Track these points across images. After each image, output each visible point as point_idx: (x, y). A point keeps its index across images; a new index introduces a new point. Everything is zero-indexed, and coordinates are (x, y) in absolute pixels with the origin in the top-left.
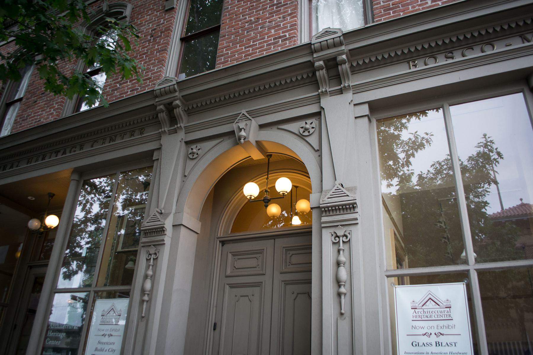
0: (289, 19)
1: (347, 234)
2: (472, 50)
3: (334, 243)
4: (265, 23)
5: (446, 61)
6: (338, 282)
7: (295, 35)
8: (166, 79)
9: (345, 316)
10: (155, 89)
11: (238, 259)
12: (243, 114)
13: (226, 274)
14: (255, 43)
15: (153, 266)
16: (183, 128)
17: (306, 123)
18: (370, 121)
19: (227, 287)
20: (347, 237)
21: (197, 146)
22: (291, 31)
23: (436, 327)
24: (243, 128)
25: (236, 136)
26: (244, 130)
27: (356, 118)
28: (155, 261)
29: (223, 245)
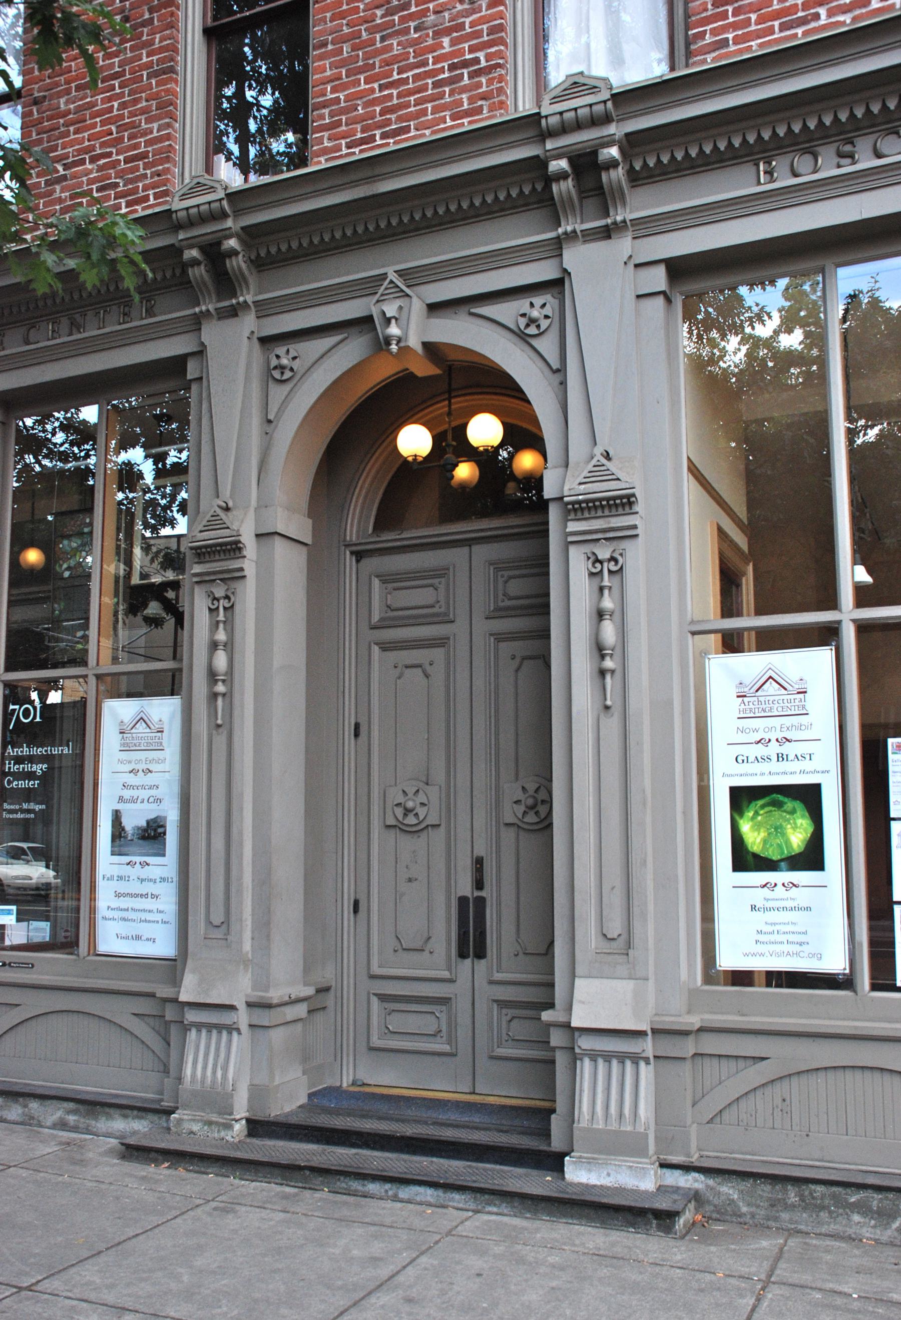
0: (484, 9)
1: (616, 555)
2: (894, 136)
3: (592, 574)
4: (424, 13)
5: (839, 166)
6: (600, 650)
7: (501, 61)
8: (198, 183)
9: (613, 709)
10: (175, 207)
11: (394, 589)
12: (391, 282)
13: (370, 621)
14: (404, 76)
15: (225, 622)
16: (252, 307)
17: (532, 305)
18: (668, 300)
19: (376, 649)
20: (616, 561)
21: (288, 350)
22: (491, 46)
23: (778, 728)
24: (394, 317)
25: (376, 329)
26: (396, 319)
27: (638, 297)
28: (229, 613)
29: (358, 561)
